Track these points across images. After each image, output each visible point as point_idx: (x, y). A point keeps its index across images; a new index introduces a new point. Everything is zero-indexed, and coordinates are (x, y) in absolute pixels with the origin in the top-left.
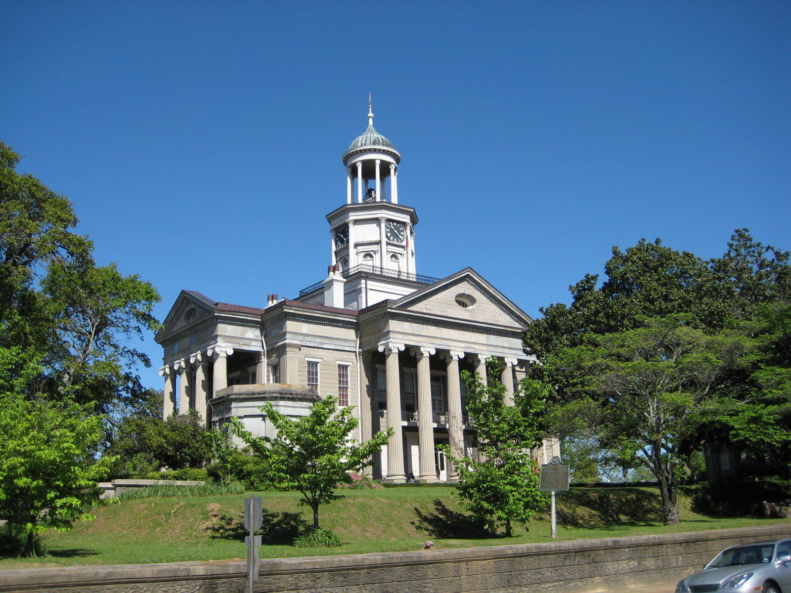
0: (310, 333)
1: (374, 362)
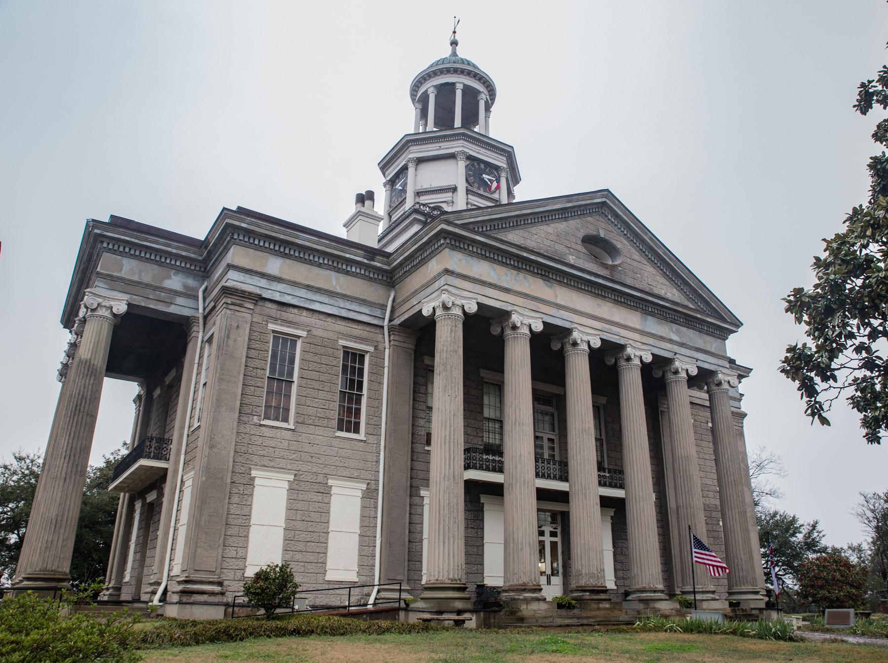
0: (284, 277)
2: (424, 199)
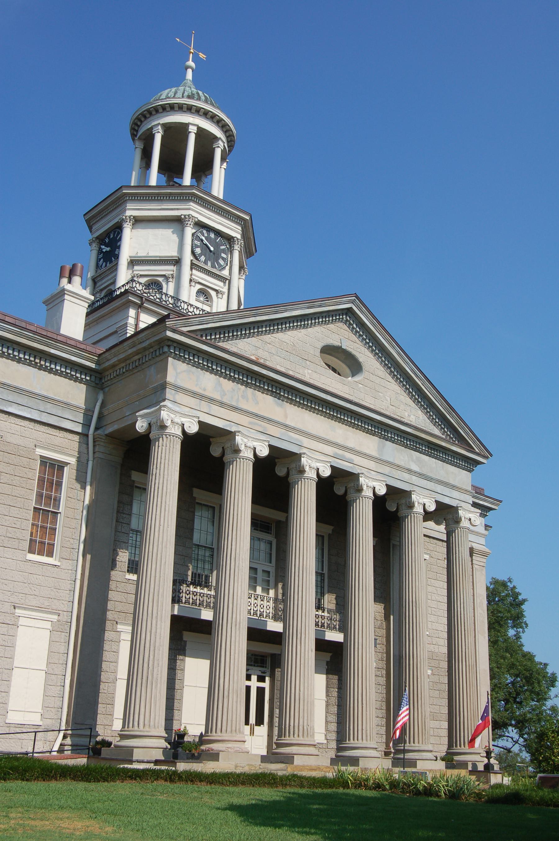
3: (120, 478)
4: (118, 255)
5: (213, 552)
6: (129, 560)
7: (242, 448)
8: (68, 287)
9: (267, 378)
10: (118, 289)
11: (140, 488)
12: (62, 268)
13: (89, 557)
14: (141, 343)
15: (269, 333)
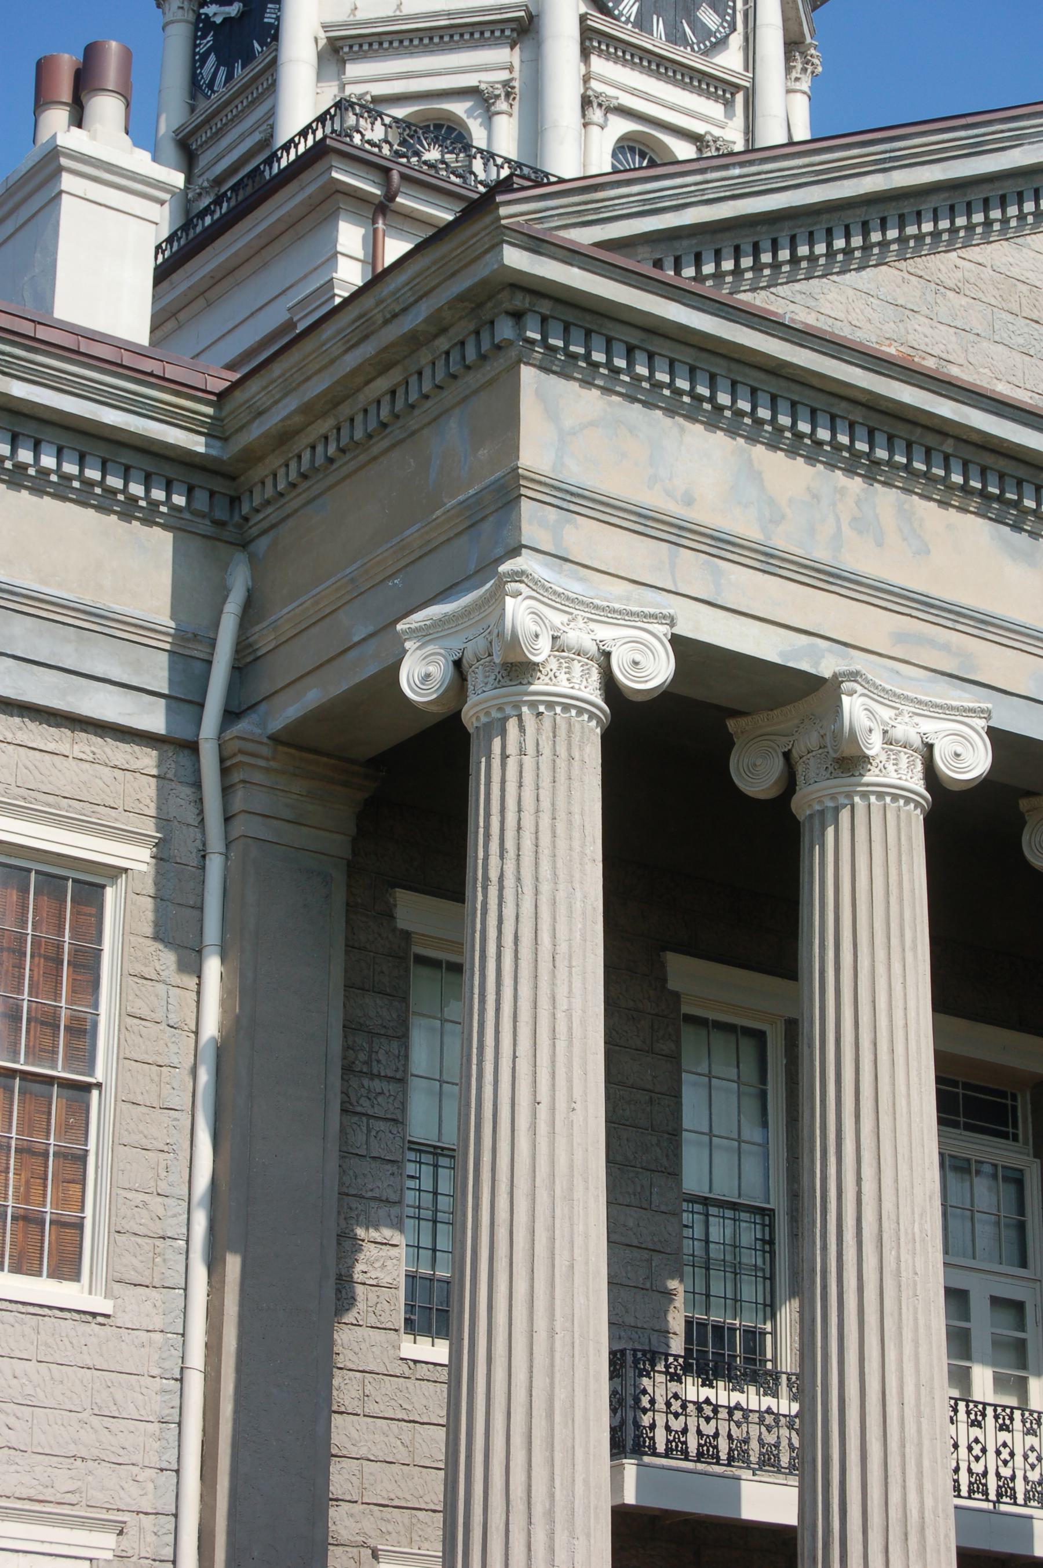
1: (365, 823)
2: (370, 78)
3: (348, 922)
4: (277, 29)
5: (772, 1226)
6: (411, 1277)
7: (874, 746)
8: (72, 139)
9: (957, 438)
10: (286, 147)
11: (434, 964)
12: (43, 69)
13: (233, 1264)
14: (395, 316)
15: (951, 242)
